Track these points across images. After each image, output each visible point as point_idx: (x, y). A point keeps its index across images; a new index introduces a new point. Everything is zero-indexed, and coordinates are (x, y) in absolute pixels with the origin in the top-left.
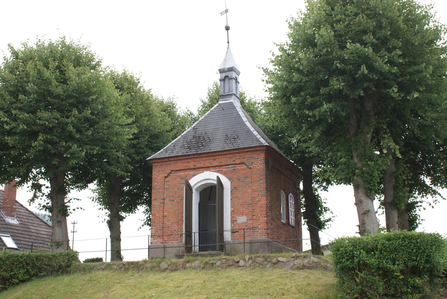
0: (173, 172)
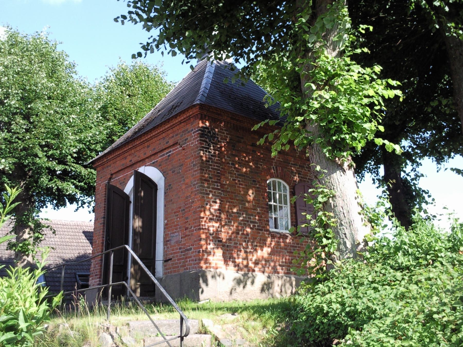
0: (114, 176)
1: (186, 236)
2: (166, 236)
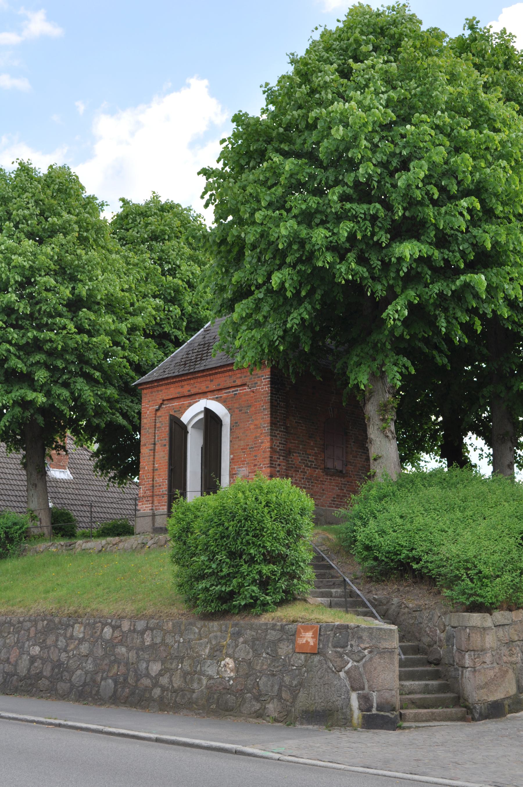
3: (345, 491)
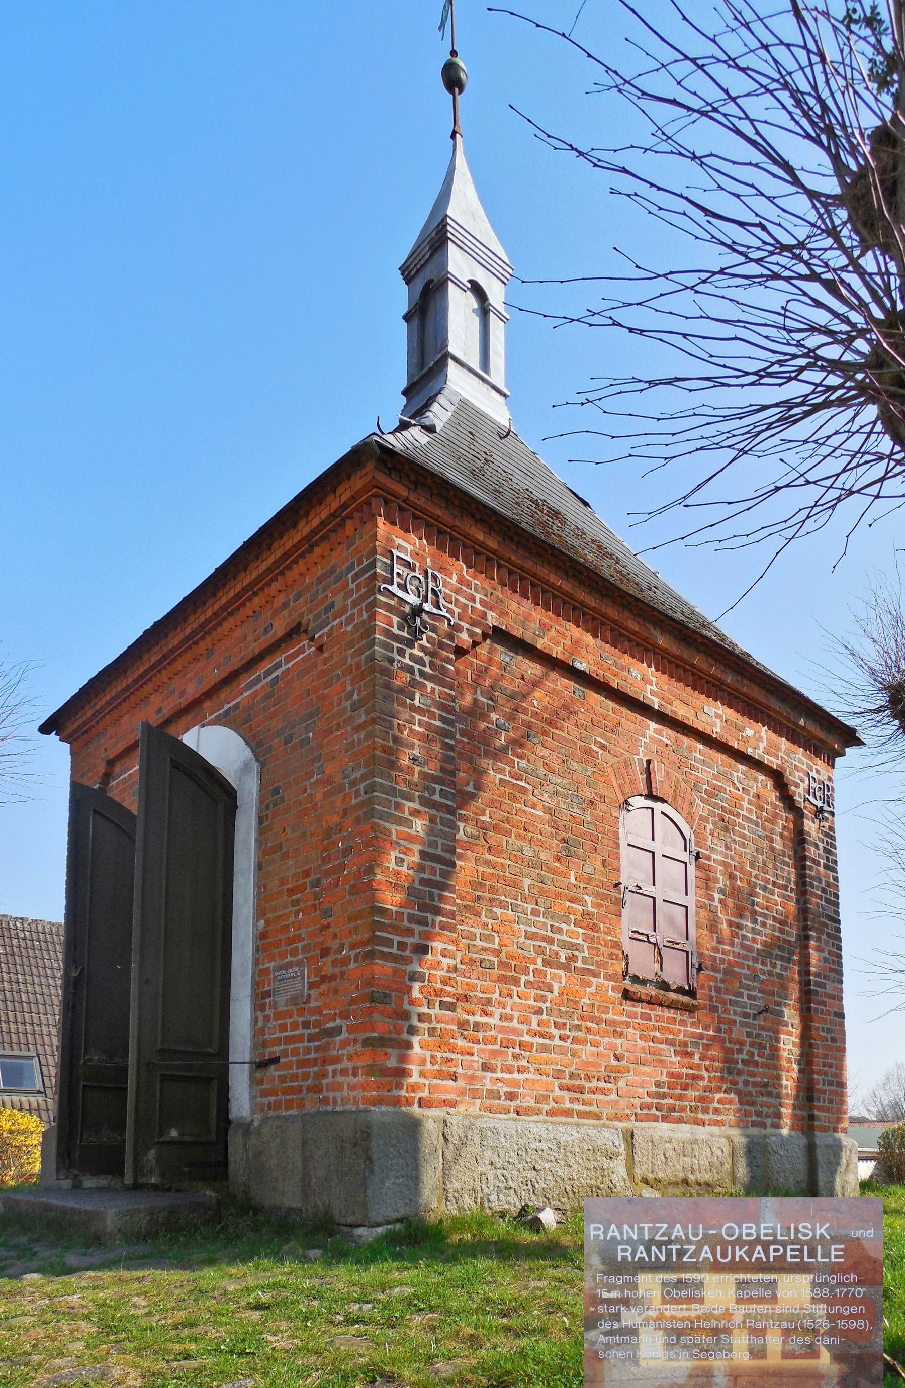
0: (117, 768)
1: (324, 979)
2: (260, 976)
3: (696, 1059)
